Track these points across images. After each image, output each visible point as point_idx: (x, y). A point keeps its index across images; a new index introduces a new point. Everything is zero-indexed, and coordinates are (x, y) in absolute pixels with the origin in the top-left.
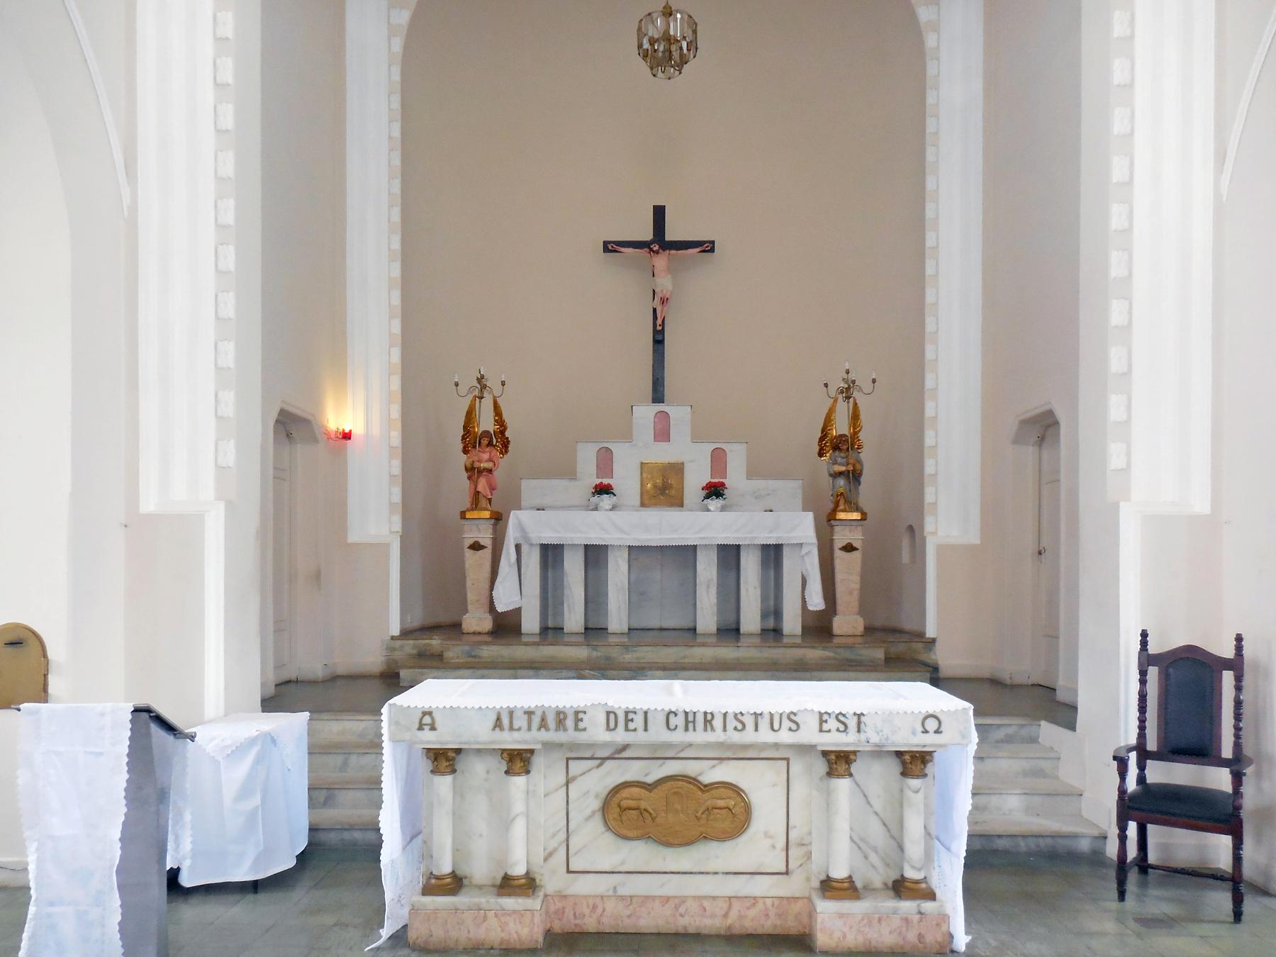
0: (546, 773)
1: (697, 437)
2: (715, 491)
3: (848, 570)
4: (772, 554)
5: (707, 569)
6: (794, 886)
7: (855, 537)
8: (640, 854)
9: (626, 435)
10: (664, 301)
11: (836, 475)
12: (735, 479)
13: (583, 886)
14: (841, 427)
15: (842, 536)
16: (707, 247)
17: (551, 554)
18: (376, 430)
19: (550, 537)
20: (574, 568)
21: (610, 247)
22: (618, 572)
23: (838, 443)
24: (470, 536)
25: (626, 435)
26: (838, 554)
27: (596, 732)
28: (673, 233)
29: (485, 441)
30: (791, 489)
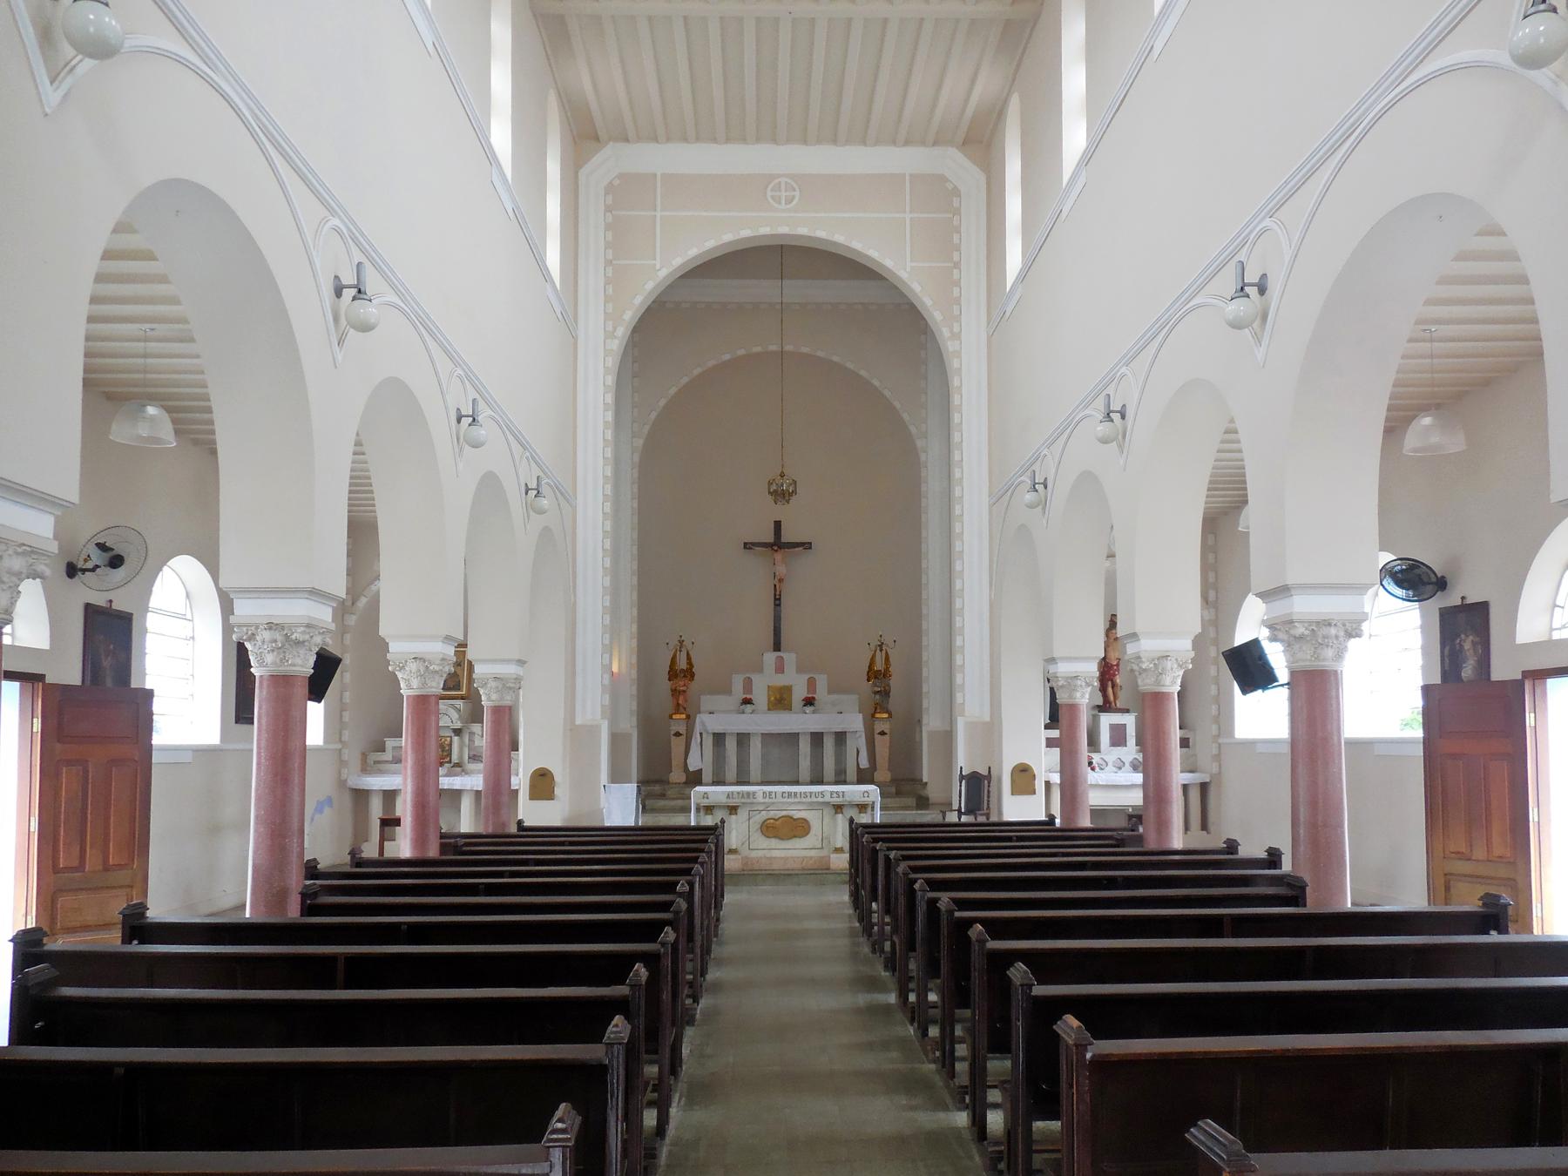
0: (743, 814)
1: (800, 670)
2: (809, 702)
3: (882, 745)
4: (840, 737)
5: (805, 746)
6: (824, 853)
7: (886, 727)
8: (774, 843)
9: (760, 670)
10: (781, 580)
11: (876, 693)
12: (821, 694)
13: (754, 854)
14: (879, 666)
15: (879, 727)
16: (807, 546)
17: (719, 738)
18: (624, 670)
19: (719, 729)
20: (731, 746)
21: (747, 546)
22: (756, 747)
23: (878, 676)
24: (674, 729)
25: (760, 670)
26: (877, 737)
27: (760, 799)
28: (787, 537)
29: (681, 674)
30: (851, 701)
